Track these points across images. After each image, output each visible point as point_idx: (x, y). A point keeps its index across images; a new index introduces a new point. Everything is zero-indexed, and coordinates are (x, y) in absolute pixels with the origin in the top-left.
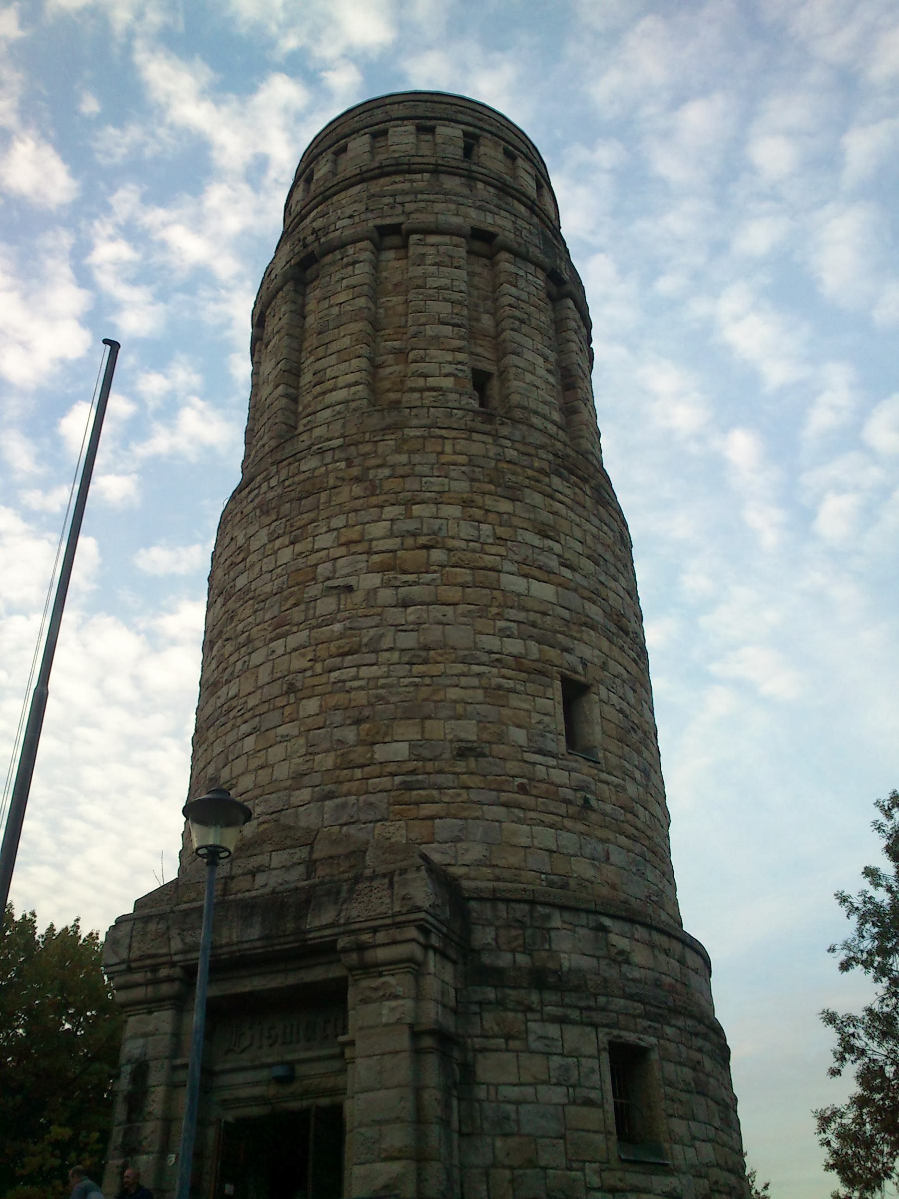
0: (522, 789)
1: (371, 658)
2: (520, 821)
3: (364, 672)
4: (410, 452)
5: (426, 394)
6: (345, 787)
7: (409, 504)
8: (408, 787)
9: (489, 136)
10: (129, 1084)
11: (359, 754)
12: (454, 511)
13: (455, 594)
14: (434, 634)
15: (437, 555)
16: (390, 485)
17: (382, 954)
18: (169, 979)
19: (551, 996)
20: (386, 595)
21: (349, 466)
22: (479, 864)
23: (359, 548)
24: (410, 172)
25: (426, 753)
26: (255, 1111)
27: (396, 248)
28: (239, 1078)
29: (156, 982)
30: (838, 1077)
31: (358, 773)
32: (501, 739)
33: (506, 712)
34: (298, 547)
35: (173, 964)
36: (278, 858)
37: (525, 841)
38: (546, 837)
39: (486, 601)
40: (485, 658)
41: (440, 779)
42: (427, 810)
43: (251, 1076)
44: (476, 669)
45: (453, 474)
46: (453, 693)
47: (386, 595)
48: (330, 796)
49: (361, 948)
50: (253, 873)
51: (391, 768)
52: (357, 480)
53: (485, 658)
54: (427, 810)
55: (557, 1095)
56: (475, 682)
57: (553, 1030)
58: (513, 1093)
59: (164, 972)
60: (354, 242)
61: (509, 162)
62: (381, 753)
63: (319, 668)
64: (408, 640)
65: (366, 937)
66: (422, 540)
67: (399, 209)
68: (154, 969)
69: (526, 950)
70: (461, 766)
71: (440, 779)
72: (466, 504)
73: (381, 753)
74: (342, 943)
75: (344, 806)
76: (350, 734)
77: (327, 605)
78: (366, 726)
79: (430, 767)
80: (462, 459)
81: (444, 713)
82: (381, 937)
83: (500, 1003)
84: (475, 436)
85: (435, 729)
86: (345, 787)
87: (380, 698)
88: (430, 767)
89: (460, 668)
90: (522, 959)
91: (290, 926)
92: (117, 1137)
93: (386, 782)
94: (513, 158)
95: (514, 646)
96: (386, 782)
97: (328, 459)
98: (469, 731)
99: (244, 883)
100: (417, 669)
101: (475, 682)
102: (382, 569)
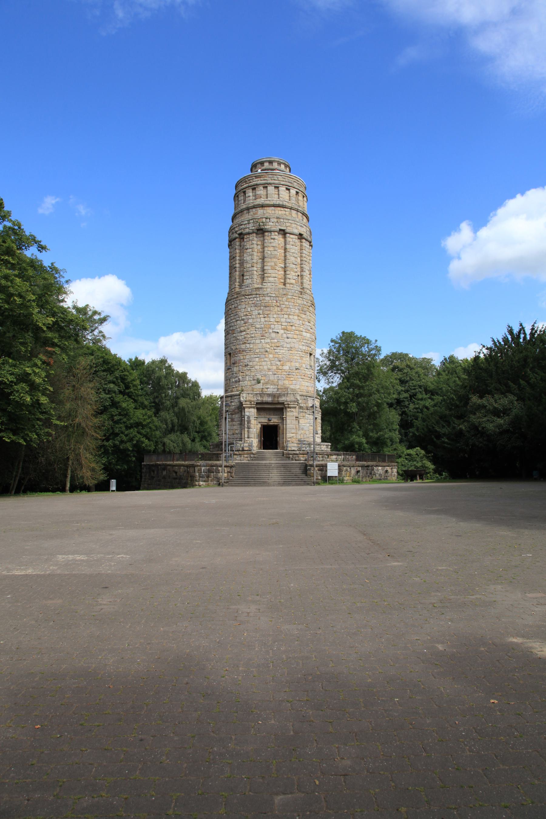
1: (282, 348)
4: (289, 302)
5: (291, 285)
6: (278, 373)
8: (289, 375)
10: (300, 442)
11: (280, 367)
12: (296, 317)
13: (295, 336)
14: (292, 345)
16: (285, 310)
17: (292, 406)
18: (254, 404)
21: (277, 302)
22: (299, 389)
23: (279, 323)
24: (285, 208)
25: (291, 369)
27: (282, 234)
30: (56, 265)
33: (303, 361)
34: (266, 319)
36: (271, 387)
37: (304, 385)
39: (301, 338)
41: (293, 374)
42: (292, 379)
44: (299, 353)
45: (296, 308)
46: (295, 357)
47: (285, 336)
49: (288, 404)
50: (267, 388)
51: (286, 371)
52: (278, 306)
53: (300, 350)
54: (292, 379)
55: (308, 425)
56: (298, 355)
58: (304, 424)
59: (253, 403)
60: (274, 232)
61: (288, 192)
62: (284, 368)
64: (288, 346)
65: (290, 403)
66: (291, 324)
67: (284, 225)
68: (251, 402)
69: (305, 404)
70: (296, 371)
71: (293, 374)
72: (298, 316)
73: (284, 368)
74: (285, 403)
75: (278, 377)
76: (278, 363)
77: (273, 335)
78: (282, 362)
79: (292, 371)
81: (294, 361)
84: (300, 298)
86: (278, 373)
87: (284, 357)
88: (292, 371)
89: (296, 352)
90: (305, 405)
92: (246, 426)
93: (285, 373)
94: (289, 190)
95: (304, 348)
96: (285, 373)
97: (272, 299)
98: (297, 365)
99: (266, 390)
100: (290, 352)
101: (298, 355)
102: (284, 329)
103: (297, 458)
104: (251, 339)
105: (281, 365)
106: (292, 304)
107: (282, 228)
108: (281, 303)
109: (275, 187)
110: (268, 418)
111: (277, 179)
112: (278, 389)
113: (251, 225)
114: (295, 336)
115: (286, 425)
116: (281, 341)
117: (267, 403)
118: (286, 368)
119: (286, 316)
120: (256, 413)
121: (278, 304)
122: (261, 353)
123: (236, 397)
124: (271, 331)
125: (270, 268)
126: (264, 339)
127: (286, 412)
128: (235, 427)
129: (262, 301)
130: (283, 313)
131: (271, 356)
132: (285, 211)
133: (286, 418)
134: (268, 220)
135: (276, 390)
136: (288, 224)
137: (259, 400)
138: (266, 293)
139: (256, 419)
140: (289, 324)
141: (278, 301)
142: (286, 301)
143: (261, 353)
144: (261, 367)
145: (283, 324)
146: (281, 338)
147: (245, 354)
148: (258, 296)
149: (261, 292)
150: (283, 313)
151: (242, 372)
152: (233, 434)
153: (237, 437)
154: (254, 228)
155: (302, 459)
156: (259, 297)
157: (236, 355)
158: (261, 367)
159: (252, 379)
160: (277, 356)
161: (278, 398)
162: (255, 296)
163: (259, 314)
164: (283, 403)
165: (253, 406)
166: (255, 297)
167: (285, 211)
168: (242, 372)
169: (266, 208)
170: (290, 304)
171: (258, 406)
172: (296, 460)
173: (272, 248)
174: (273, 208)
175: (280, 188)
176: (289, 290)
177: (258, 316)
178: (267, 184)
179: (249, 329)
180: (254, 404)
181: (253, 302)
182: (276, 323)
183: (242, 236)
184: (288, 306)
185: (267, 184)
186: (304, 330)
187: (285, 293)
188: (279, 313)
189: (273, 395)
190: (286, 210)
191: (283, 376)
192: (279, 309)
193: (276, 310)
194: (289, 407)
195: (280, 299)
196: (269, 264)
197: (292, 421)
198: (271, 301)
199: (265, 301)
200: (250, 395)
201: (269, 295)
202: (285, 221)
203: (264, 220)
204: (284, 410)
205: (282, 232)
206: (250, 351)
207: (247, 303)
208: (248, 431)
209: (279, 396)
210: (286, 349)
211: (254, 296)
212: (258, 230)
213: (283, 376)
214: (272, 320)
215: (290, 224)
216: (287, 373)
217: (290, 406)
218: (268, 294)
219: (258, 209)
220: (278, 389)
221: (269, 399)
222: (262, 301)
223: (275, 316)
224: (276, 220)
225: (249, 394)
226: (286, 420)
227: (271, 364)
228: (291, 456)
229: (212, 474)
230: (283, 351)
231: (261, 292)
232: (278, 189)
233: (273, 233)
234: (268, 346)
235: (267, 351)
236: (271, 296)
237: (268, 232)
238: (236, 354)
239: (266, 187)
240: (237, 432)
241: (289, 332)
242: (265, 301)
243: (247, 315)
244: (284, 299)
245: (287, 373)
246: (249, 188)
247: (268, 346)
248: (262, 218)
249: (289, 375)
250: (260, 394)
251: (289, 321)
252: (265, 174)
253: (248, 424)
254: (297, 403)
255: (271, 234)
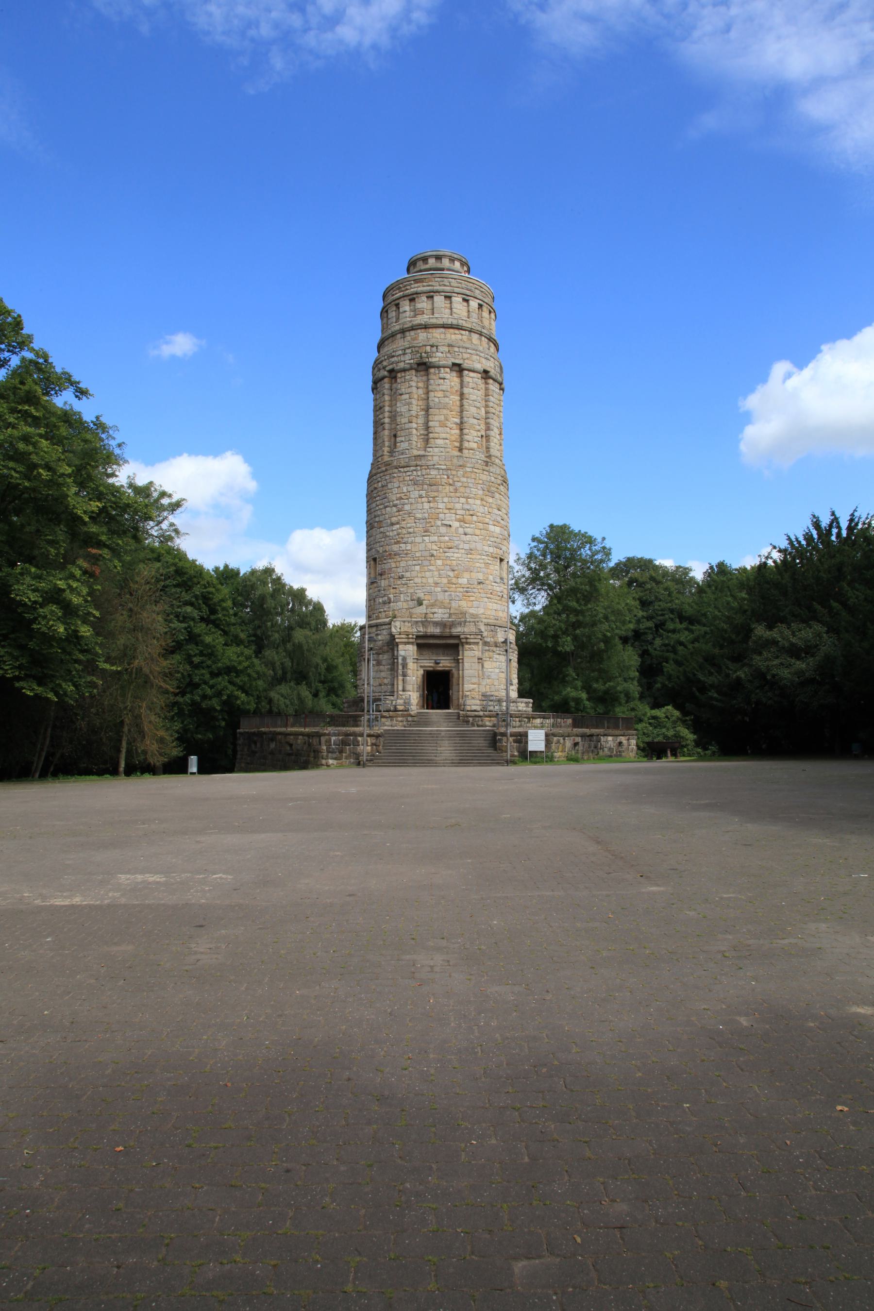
0: (491, 593)
1: (457, 551)
2: (490, 602)
3: (456, 555)
5: (471, 451)
7: (468, 498)
8: (467, 592)
9: (456, 295)
11: (454, 580)
12: (478, 502)
13: (478, 532)
14: (473, 546)
15: (475, 518)
16: (462, 490)
17: (472, 641)
18: (412, 638)
19: (498, 649)
20: (461, 530)
21: (448, 478)
23: (453, 511)
24: (461, 329)
26: (431, 669)
28: (425, 661)
29: (409, 638)
30: (103, 419)
31: (454, 586)
32: (487, 579)
33: (489, 571)
34: (432, 505)
35: (413, 635)
36: (440, 611)
38: (495, 606)
40: (485, 553)
41: (474, 590)
42: (472, 599)
43: (428, 661)
44: (483, 557)
45: (479, 488)
46: (477, 565)
47: (461, 530)
48: (446, 591)
49: (467, 638)
50: (433, 613)
51: (463, 586)
52: (450, 485)
53: (485, 553)
54: (472, 599)
55: (497, 671)
57: (497, 656)
58: (490, 670)
59: (411, 636)
60: (444, 367)
62: (460, 581)
63: (441, 550)
64: (467, 546)
65: (468, 636)
66: (471, 513)
68: (407, 635)
69: (493, 637)
70: (479, 587)
71: (474, 590)
72: (482, 500)
73: (460, 581)
74: (462, 636)
75: (451, 595)
76: (451, 574)
77: (443, 530)
80: (481, 482)
81: (475, 571)
82: (472, 636)
83: (489, 650)
85: (474, 575)
89: (479, 557)
90: (492, 640)
91: (448, 631)
92: (400, 672)
93: (461, 590)
95: (491, 550)
96: (461, 590)
97: (441, 473)
98: (481, 576)
99: (431, 616)
103: (480, 723)
104: (408, 536)
105: (455, 577)
106: (473, 481)
107: (457, 361)
108: (456, 479)
109: (446, 297)
110: (435, 660)
111: (448, 284)
112: (450, 614)
113: (408, 357)
114: (478, 532)
115: (463, 670)
116: (455, 538)
117: (433, 637)
118: (463, 581)
119: (463, 500)
120: (415, 652)
121: (451, 481)
122: (423, 558)
123: (384, 627)
124: (439, 523)
125: (437, 424)
126: (429, 536)
127: (463, 651)
128: (383, 674)
129: (425, 477)
130: (458, 495)
131: (439, 562)
132: (462, 335)
133: (463, 659)
134: (434, 349)
135: (447, 615)
136: (466, 356)
137: (420, 632)
138: (431, 463)
139: (415, 661)
140: (467, 513)
141: (451, 477)
142: (463, 477)
143: (423, 558)
144: (424, 580)
145: (459, 512)
146: (455, 535)
147: (399, 559)
148: (419, 468)
149: (423, 462)
150: (458, 495)
151: (393, 588)
152: (380, 685)
153: (385, 690)
154: (412, 361)
155: (488, 723)
156: (421, 470)
157: (385, 562)
158: (424, 580)
159: (409, 599)
160: (449, 562)
161: (450, 629)
162: (414, 468)
163: (421, 497)
164: (458, 637)
165: (411, 640)
166: (415, 470)
167: (462, 335)
168: (393, 588)
169: (430, 330)
170: (469, 480)
171: (419, 641)
172: (478, 726)
173: (441, 392)
174: (442, 330)
175: (453, 299)
176: (467, 459)
177: (419, 499)
178: (433, 292)
179: (404, 520)
180: (412, 638)
181: (411, 478)
182: (447, 511)
183: (393, 374)
184: (466, 485)
185: (433, 292)
186: (491, 523)
187: (461, 463)
188: (452, 494)
189: (442, 624)
190: (463, 332)
191: (458, 594)
192: (452, 489)
193: (447, 490)
194: (467, 643)
195: (454, 473)
196: (436, 418)
197: (473, 664)
198: (439, 477)
199: (429, 476)
200: (406, 624)
201: (436, 467)
202: (461, 350)
203: (428, 348)
204: (460, 648)
205: (457, 368)
206: (406, 554)
207: (401, 479)
208: (403, 680)
209: (453, 625)
210: (463, 551)
211: (412, 468)
212: (419, 364)
213: (458, 594)
214: (441, 506)
215: (468, 356)
216: (465, 589)
217: (468, 640)
218: (434, 465)
219: (419, 331)
220: (450, 614)
221: (437, 631)
222: (425, 477)
223: (446, 500)
224: (446, 349)
225: (404, 622)
226: (463, 662)
227: (439, 575)
228: (471, 719)
229: (348, 747)
230: (459, 555)
231: (423, 462)
232: (451, 301)
233: (442, 369)
234: (435, 547)
235: (432, 555)
236: (438, 469)
237: (434, 367)
238: (385, 559)
239: (432, 297)
240: (386, 681)
241: (467, 525)
242: (429, 476)
243: (401, 498)
244: (461, 473)
245: (465, 589)
246: (405, 298)
247: (435, 547)
248: (426, 346)
249: (467, 592)
250: (422, 622)
251: (468, 507)
252: (429, 276)
253: (403, 669)
254: (480, 637)
255: (440, 371)
